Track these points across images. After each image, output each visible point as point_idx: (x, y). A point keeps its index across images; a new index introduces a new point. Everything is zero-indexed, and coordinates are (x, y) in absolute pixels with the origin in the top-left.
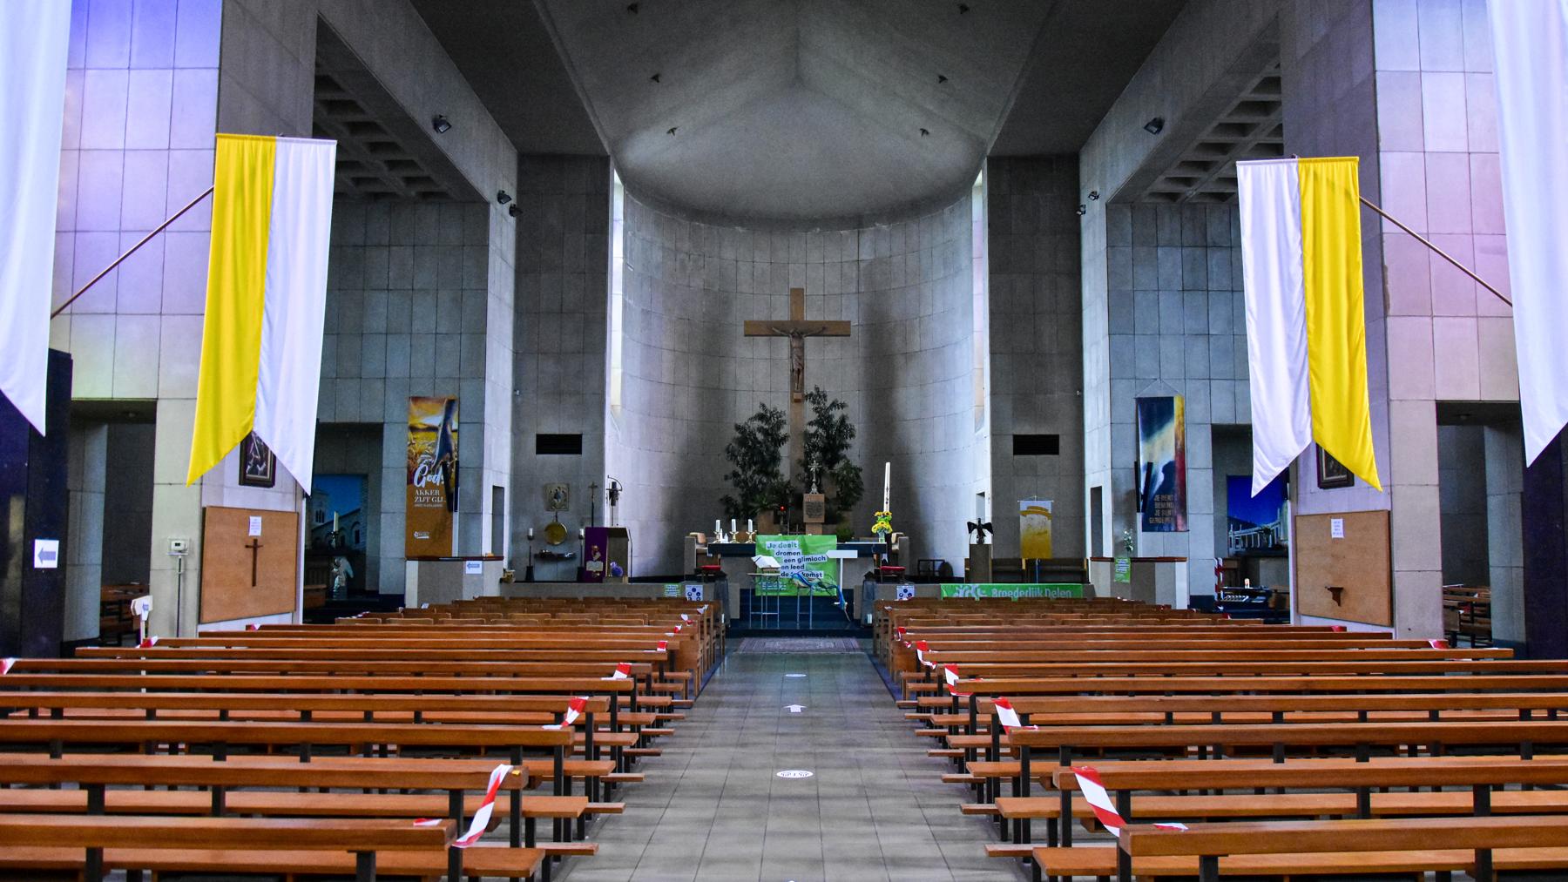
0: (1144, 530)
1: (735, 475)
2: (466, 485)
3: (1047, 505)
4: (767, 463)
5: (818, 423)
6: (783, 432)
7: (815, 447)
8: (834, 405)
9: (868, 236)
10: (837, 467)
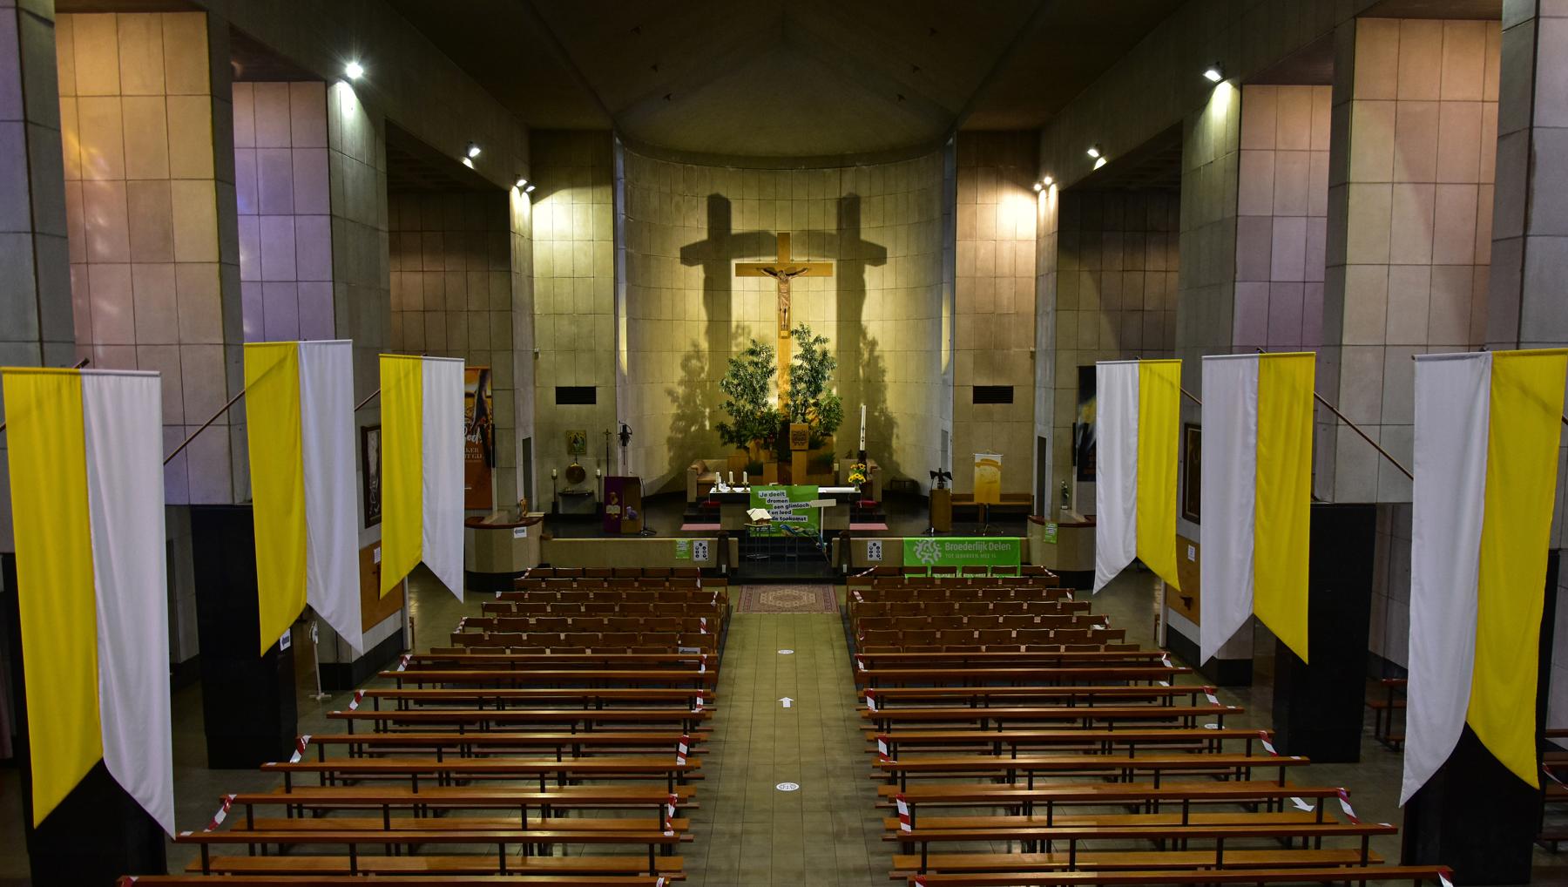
0: (1079, 479)
1: (729, 404)
2: (502, 448)
3: (998, 458)
4: (756, 391)
5: (803, 357)
6: (771, 365)
7: (801, 379)
8: (817, 340)
9: (849, 175)
10: (821, 396)
